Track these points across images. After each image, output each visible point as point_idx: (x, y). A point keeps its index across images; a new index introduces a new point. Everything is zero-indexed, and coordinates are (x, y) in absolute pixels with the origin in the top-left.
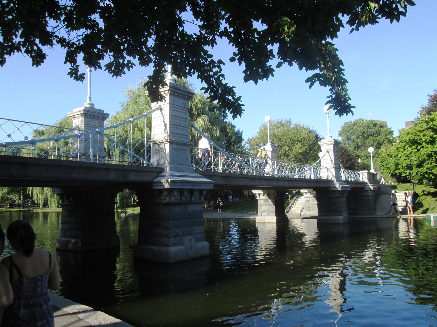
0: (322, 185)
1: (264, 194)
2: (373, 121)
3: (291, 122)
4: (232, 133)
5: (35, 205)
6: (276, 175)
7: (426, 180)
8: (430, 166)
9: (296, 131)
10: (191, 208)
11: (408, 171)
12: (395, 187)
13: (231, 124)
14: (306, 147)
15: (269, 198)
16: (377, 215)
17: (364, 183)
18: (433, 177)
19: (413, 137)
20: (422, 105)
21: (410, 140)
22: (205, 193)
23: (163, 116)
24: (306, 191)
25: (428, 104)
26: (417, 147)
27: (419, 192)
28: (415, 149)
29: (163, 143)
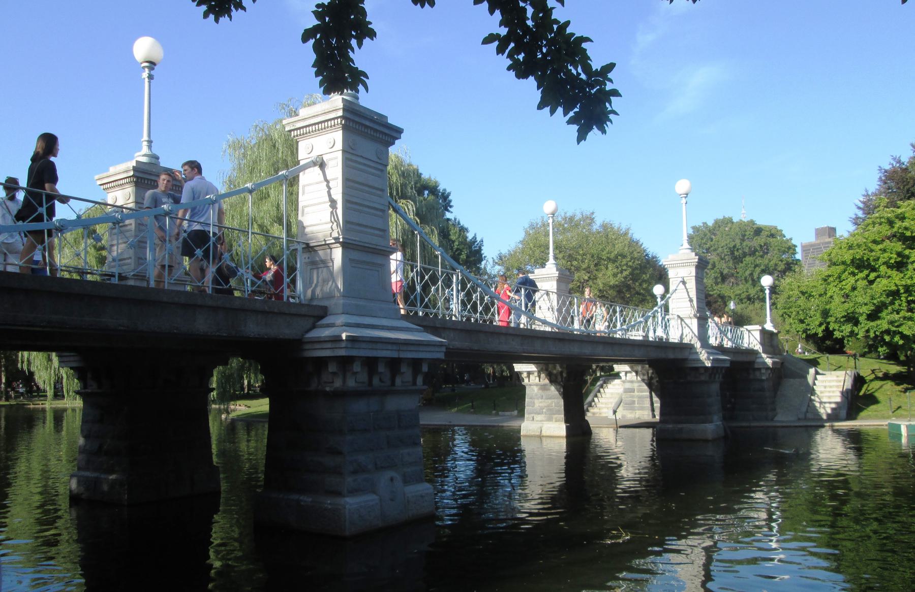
0: (671, 355)
1: (539, 373)
2: (752, 222)
3: (592, 219)
4: (461, 243)
5: (33, 390)
6: (577, 330)
7: (885, 348)
8: (896, 317)
9: (604, 239)
10: (393, 404)
11: (847, 328)
12: (814, 363)
13: (459, 223)
14: (625, 273)
15: (551, 381)
16: (779, 421)
17: (752, 352)
18: (901, 342)
19: (859, 253)
20: (866, 191)
21: (853, 261)
22: (425, 368)
23: (328, 182)
24: (626, 368)
25: (877, 187)
26: (868, 276)
27: (865, 373)
28: (863, 279)
29: (328, 246)
